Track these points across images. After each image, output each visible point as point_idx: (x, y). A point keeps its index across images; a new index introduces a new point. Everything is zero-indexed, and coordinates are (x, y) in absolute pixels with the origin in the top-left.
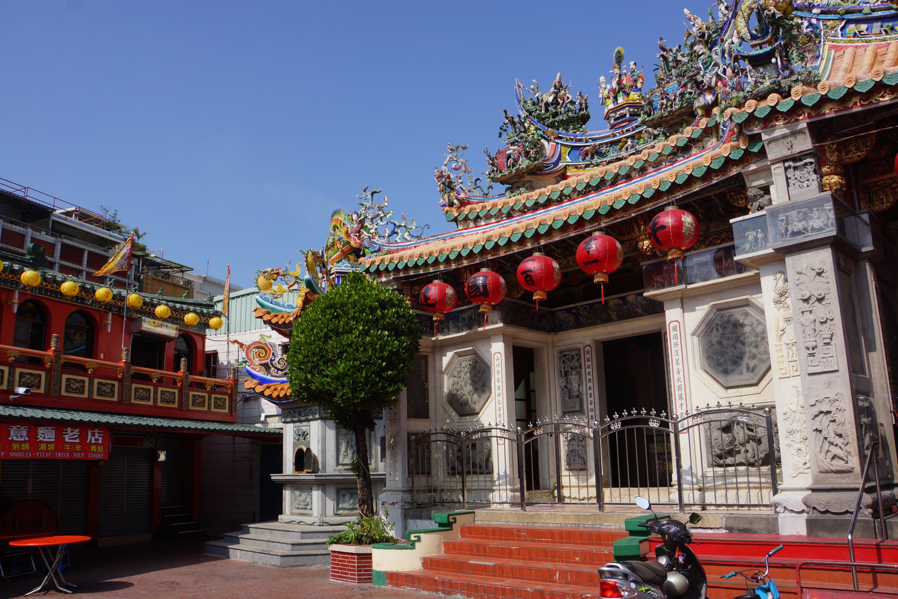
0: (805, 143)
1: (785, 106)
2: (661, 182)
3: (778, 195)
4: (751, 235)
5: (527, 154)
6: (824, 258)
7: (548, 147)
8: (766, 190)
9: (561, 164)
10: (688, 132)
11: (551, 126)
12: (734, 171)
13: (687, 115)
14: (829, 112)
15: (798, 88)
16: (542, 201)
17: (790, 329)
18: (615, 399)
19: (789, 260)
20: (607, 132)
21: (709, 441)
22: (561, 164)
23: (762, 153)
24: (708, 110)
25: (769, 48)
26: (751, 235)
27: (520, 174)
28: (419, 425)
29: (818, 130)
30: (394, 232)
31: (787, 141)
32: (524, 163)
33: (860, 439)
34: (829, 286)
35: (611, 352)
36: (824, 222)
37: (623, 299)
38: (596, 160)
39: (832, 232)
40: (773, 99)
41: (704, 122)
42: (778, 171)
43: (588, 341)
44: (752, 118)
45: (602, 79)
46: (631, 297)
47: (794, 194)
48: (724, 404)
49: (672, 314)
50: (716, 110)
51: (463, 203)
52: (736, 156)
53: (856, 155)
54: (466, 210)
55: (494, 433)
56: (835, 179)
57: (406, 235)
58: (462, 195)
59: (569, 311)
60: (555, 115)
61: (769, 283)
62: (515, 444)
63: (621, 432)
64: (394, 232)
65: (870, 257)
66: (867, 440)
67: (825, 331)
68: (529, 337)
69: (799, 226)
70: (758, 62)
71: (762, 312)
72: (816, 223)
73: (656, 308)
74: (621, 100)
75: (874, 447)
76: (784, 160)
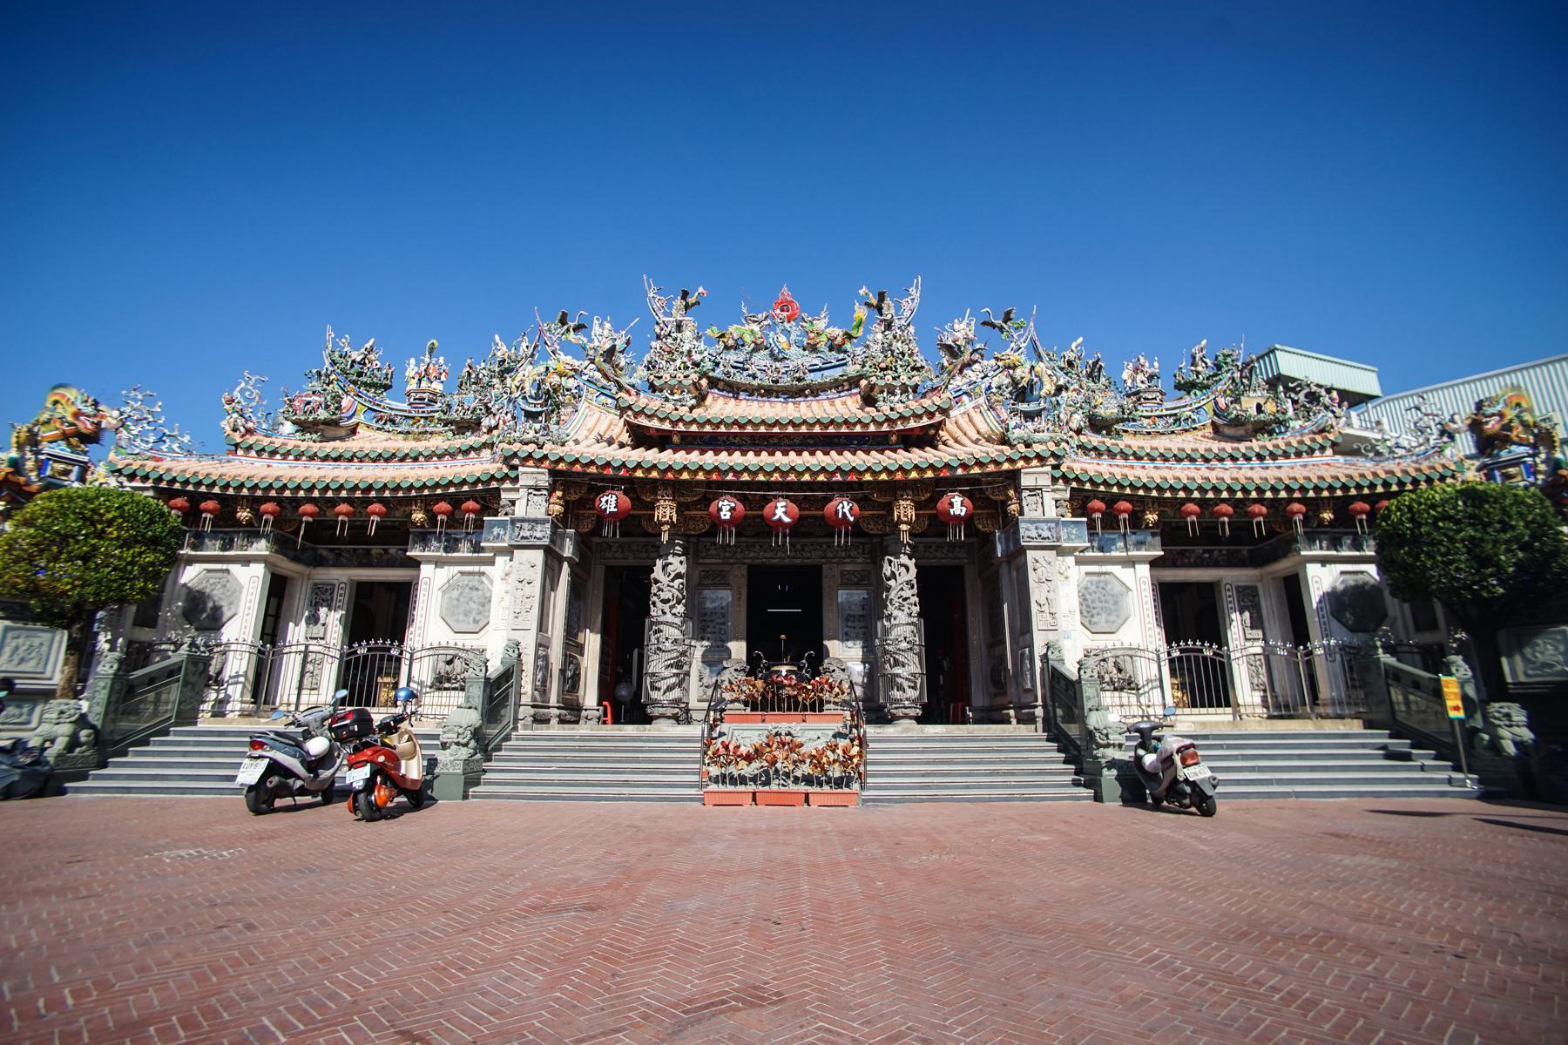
0: (544, 480)
1: (538, 454)
2: (443, 478)
3: (520, 511)
4: (496, 530)
5: (327, 407)
6: (538, 556)
7: (346, 402)
8: (513, 503)
9: (354, 420)
10: (470, 439)
11: (355, 383)
12: (494, 484)
13: (472, 426)
14: (561, 466)
15: (548, 446)
16: (334, 455)
17: (507, 598)
18: (356, 630)
19: (516, 552)
20: (405, 406)
21: (435, 669)
22: (354, 420)
23: (516, 480)
24: (490, 430)
25: (539, 409)
26: (496, 530)
27: (316, 423)
28: (145, 634)
29: (553, 473)
30: (161, 440)
31: (532, 476)
32: (323, 414)
33: (535, 674)
34: (537, 575)
35: (363, 591)
36: (543, 533)
37: (386, 551)
38: (388, 426)
39: (546, 542)
40: (531, 448)
41: (484, 438)
42: (523, 492)
43: (344, 579)
44: (515, 455)
45: (413, 361)
46: (393, 550)
47: (530, 503)
48: (452, 644)
49: (426, 570)
50: (495, 432)
51: (249, 431)
52: (498, 476)
53: (574, 497)
54: (251, 440)
55: (233, 647)
56: (558, 507)
57: (175, 446)
58: (250, 425)
59: (332, 550)
60: (360, 374)
61: (500, 560)
62: (254, 658)
63: (366, 657)
64: (161, 440)
65: (569, 560)
66: (539, 676)
67: (528, 603)
68: (287, 566)
69: (527, 534)
70: (531, 416)
71: (492, 582)
72: (539, 535)
73: (415, 564)
74: (424, 384)
75: (544, 681)
76: (530, 487)
